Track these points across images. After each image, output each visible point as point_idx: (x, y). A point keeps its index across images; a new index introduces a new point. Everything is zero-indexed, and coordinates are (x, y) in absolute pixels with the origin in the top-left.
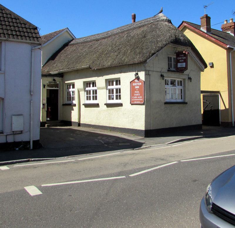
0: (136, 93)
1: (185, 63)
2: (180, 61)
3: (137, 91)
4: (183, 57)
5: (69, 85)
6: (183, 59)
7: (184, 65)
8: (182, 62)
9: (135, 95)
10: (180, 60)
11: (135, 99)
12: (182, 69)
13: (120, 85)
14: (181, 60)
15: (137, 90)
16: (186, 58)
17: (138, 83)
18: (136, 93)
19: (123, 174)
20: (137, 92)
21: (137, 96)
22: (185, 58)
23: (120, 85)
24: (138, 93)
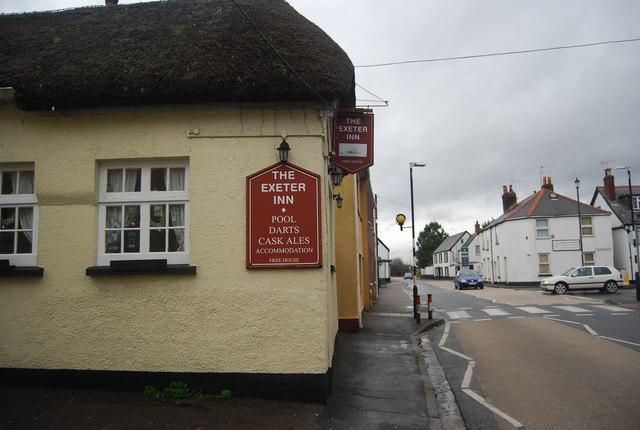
0: (276, 225)
1: (365, 146)
2: (351, 137)
3: (284, 215)
4: (290, 182)
5: (358, 347)
6: (290, 193)
7: (361, 150)
8: (356, 142)
9: (272, 230)
10: (277, 194)
11: (276, 247)
12: (353, 162)
13: (140, 190)
14: (281, 194)
15: (284, 210)
16: (336, 149)
17: (286, 185)
18: (276, 225)
19: (425, 249)
20: (283, 219)
21: (285, 237)
22: (365, 129)
23: (140, 190)
24: (290, 224)
